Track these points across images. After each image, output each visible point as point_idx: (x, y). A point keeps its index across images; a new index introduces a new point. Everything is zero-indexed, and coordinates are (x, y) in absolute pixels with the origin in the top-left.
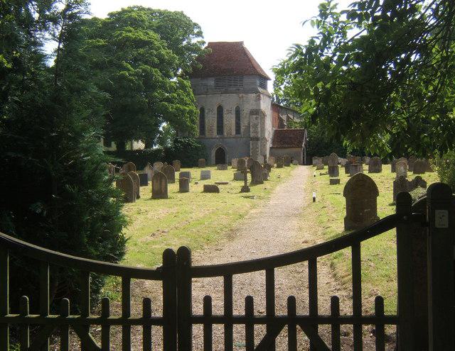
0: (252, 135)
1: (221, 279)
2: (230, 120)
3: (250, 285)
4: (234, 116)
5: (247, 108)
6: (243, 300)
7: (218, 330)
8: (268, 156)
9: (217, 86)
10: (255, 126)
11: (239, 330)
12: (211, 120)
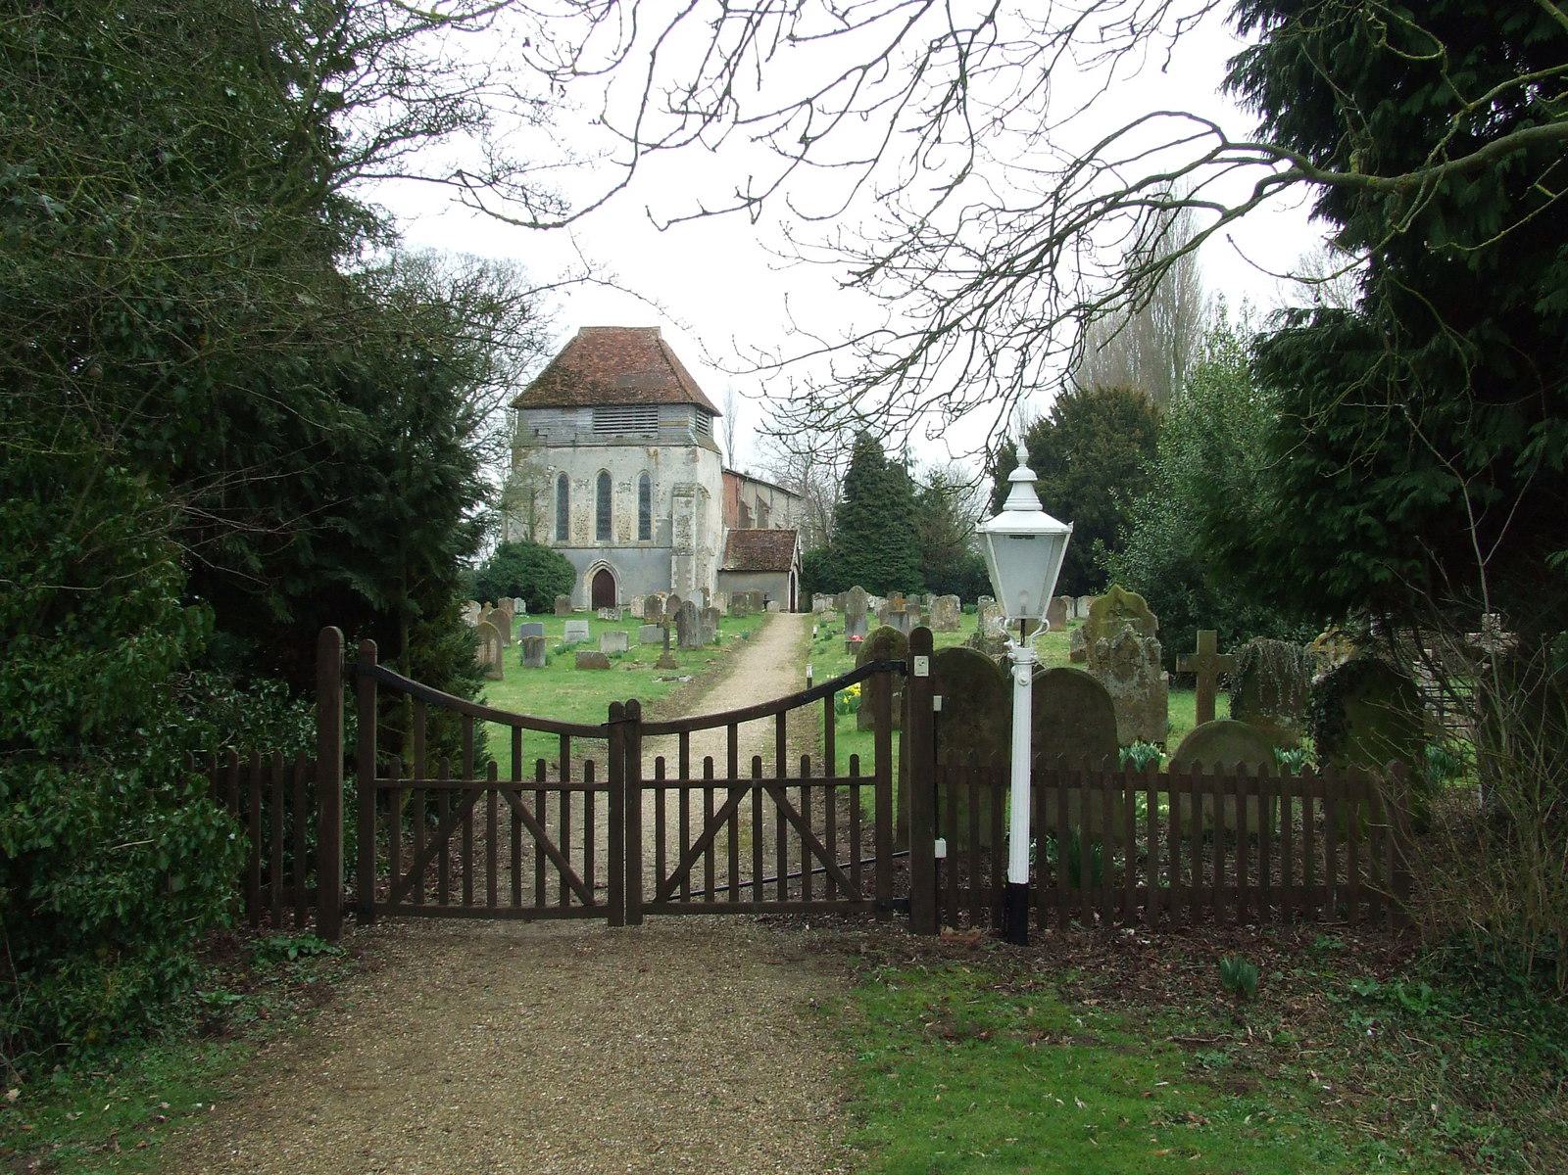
0: (676, 541)
1: (676, 737)
2: (624, 506)
3: (709, 743)
4: (635, 498)
5: (666, 479)
7: (672, 796)
8: (712, 590)
9: (597, 428)
10: (685, 521)
11: (696, 796)
12: (583, 504)
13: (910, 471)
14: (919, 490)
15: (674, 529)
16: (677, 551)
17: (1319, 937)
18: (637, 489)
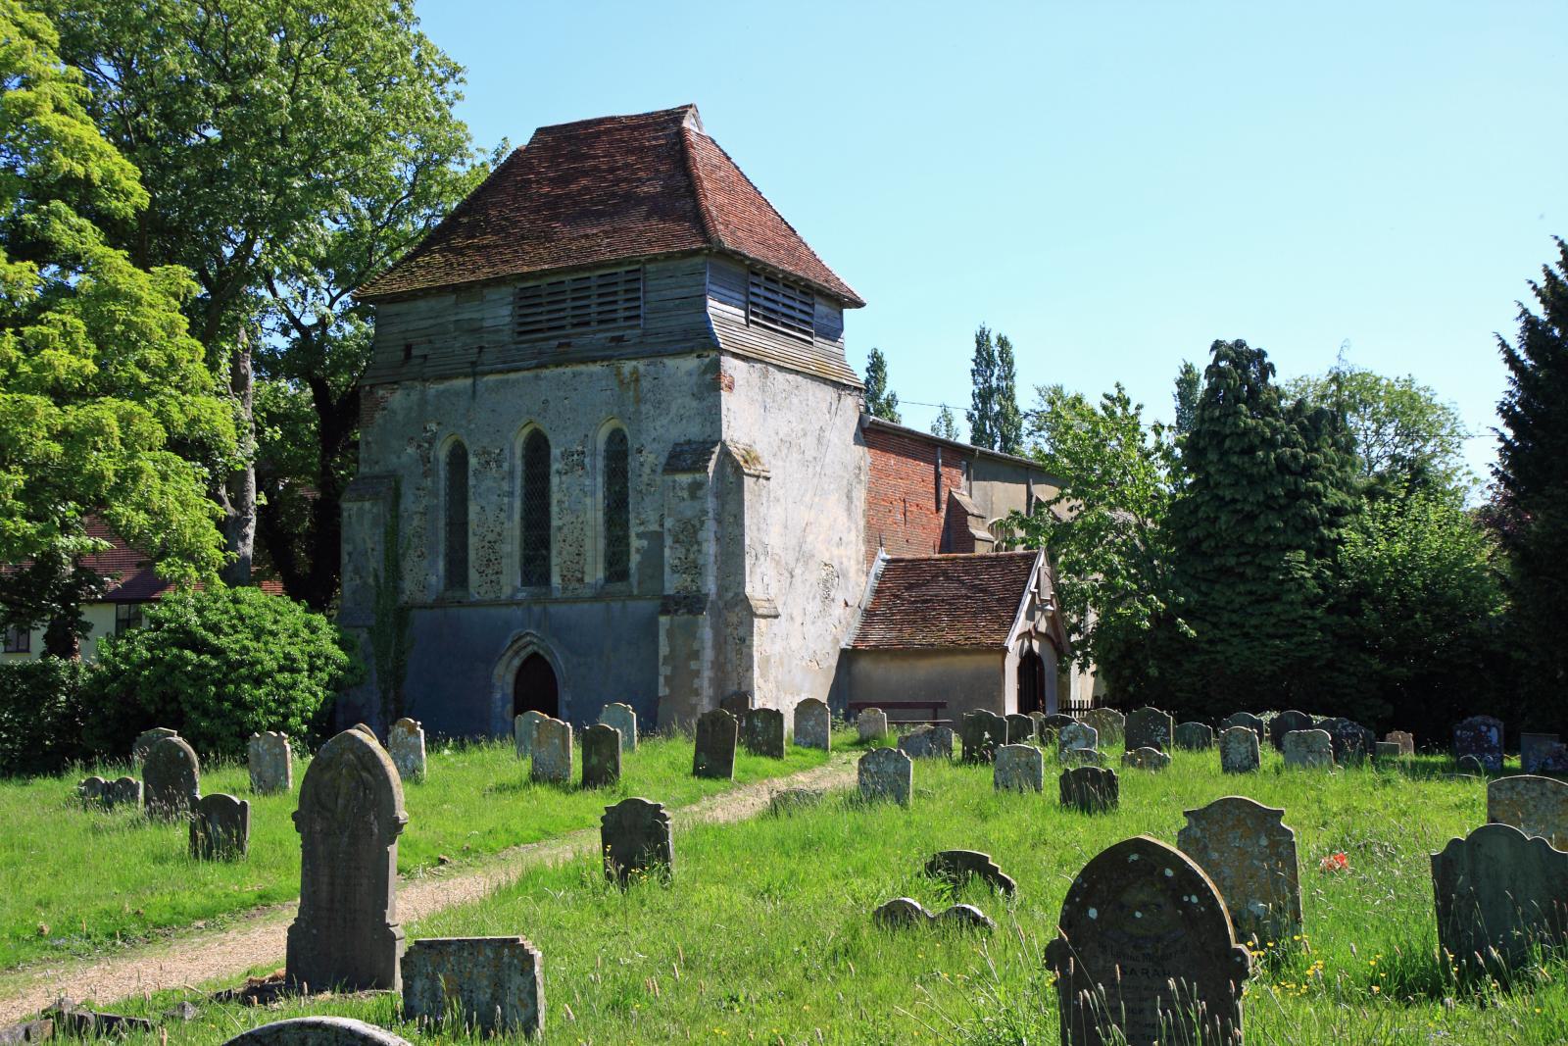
4: (598, 484)
6: (250, 846)
13: (467, 144)
14: (1475, 490)
15: (667, 552)
16: (670, 605)
17: (1331, 491)
18: (600, 463)
